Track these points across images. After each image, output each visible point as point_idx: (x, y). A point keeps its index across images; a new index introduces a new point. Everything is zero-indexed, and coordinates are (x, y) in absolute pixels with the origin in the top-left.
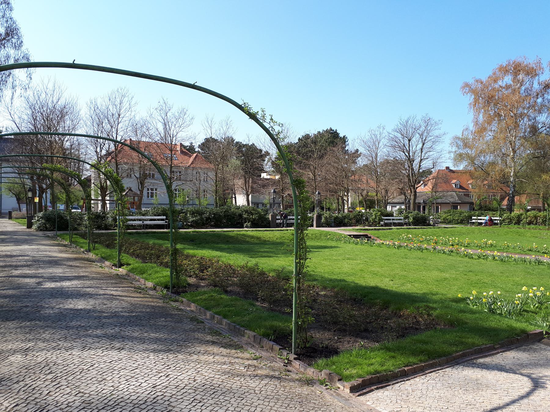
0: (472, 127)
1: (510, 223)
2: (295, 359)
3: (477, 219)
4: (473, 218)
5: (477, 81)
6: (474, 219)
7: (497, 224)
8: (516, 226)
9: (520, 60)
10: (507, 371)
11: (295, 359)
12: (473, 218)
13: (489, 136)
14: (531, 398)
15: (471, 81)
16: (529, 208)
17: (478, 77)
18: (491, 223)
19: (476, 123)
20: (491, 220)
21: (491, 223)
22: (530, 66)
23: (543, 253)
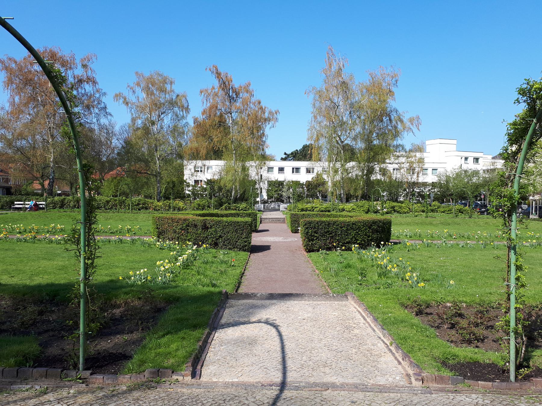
0: (7, 107)
1: (54, 207)
2: (91, 374)
3: (24, 204)
4: (15, 203)
5: (10, 59)
6: (18, 204)
7: (43, 208)
8: (62, 210)
9: (55, 50)
10: (233, 325)
11: (91, 374)
12: (15, 203)
13: (26, 118)
14: (283, 334)
15: (229, 76)
16: (59, 192)
17: (11, 56)
18: (36, 207)
19: (13, 104)
20: (36, 205)
21: (36, 207)
22: (65, 58)
23: (111, 233)
